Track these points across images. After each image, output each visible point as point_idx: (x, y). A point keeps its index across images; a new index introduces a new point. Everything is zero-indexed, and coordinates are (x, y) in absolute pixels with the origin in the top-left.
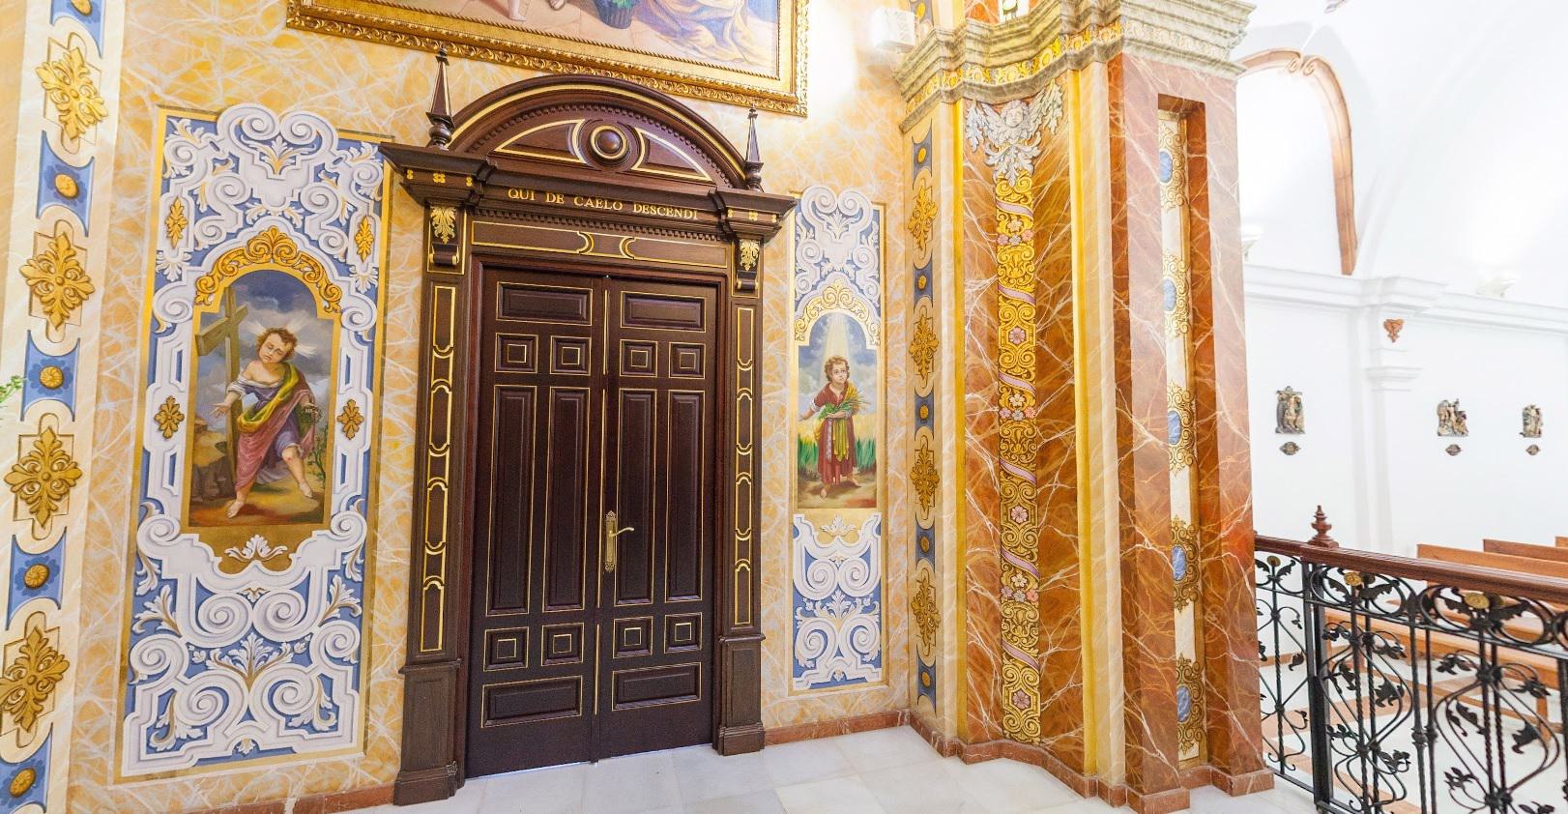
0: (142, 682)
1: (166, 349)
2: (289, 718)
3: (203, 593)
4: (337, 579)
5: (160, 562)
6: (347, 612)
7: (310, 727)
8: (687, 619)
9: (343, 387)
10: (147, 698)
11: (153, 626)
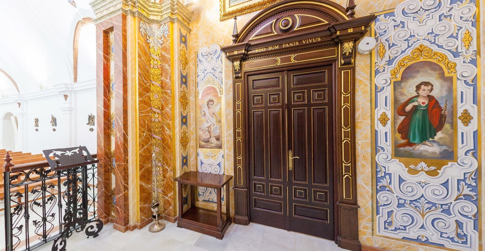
0: (381, 206)
1: (381, 97)
2: (442, 233)
3: (401, 180)
4: (462, 183)
5: (385, 167)
6: (467, 197)
7: (452, 239)
8: (278, 186)
9: (459, 105)
10: (384, 211)
11: (383, 188)
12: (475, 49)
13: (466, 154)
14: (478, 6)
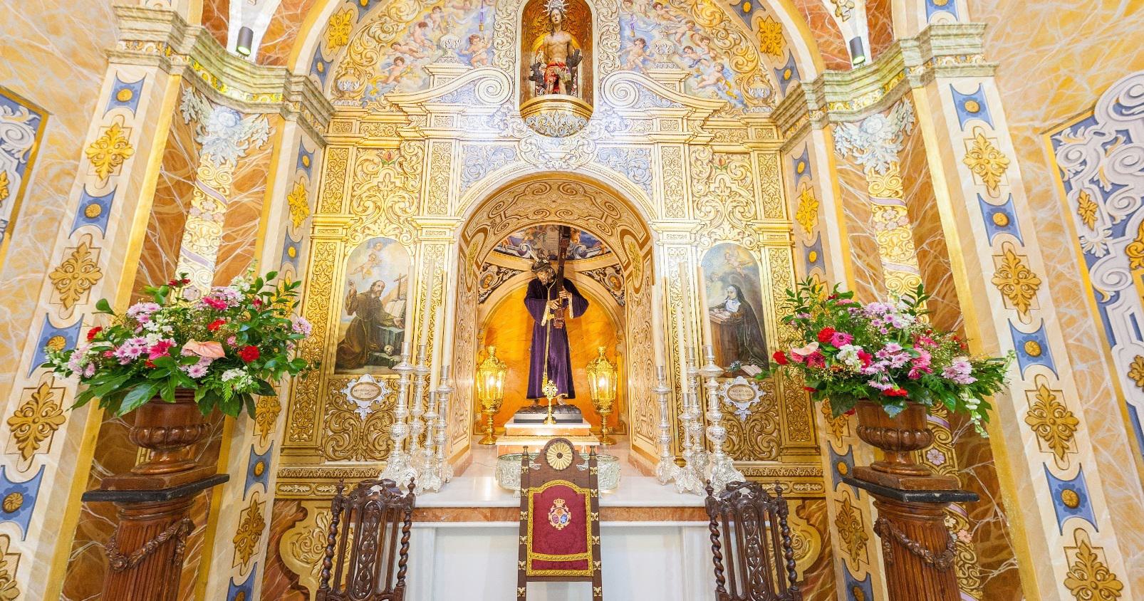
12: (7, 218)
13: (1118, 293)
14: (38, 138)
